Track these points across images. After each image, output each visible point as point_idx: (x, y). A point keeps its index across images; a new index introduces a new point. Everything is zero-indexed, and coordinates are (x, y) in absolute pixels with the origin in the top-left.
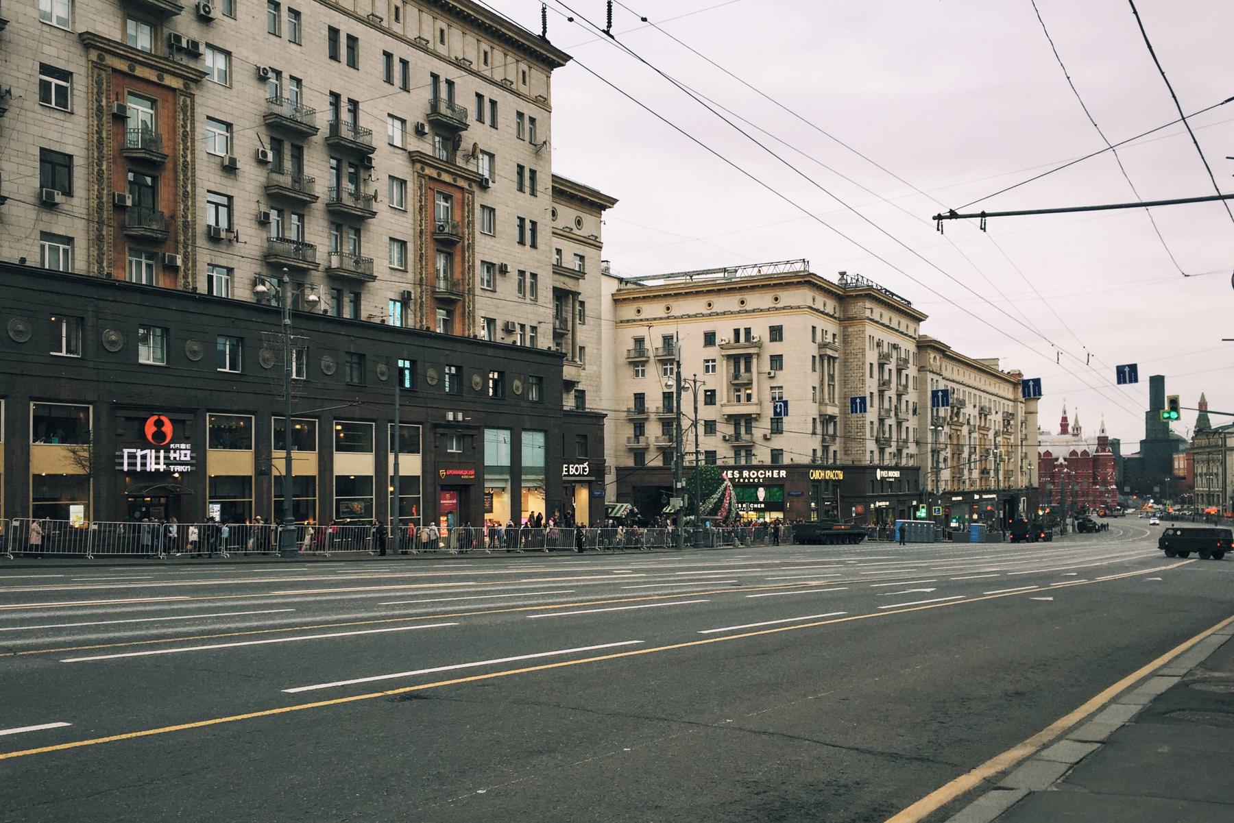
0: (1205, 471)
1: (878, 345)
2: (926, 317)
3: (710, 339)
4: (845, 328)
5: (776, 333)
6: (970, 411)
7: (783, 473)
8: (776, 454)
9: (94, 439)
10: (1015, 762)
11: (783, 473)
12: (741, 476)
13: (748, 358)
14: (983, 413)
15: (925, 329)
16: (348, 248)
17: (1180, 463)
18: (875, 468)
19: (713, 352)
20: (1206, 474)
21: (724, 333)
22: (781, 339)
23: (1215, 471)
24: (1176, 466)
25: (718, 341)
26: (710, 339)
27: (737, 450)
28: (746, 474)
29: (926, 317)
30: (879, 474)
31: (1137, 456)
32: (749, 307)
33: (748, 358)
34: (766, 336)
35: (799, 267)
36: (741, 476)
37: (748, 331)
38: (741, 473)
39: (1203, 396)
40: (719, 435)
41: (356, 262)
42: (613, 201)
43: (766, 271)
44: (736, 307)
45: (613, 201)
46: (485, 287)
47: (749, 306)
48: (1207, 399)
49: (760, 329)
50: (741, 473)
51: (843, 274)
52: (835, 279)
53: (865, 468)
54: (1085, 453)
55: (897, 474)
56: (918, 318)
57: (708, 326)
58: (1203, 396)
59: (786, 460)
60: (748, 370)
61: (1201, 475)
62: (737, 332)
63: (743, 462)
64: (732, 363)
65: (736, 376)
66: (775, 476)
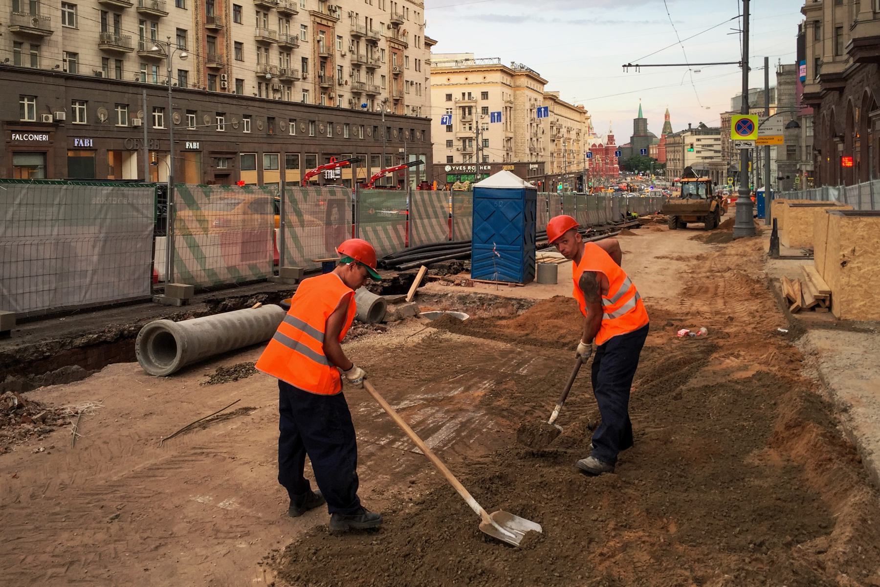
0: (672, 157)
1: (530, 100)
2: (547, 82)
3: (449, 97)
4: (515, 91)
5: (485, 95)
6: (563, 131)
7: (489, 167)
8: (485, 158)
9: (188, 120)
10: (599, 335)
11: (489, 167)
12: (467, 169)
13: (470, 108)
14: (569, 131)
15: (547, 89)
16: (263, 61)
17: (653, 151)
18: (529, 163)
19: (450, 104)
20: (673, 160)
21: (457, 95)
22: (487, 98)
23: (678, 157)
24: (651, 152)
25: (453, 98)
26: (449, 97)
27: (464, 155)
28: (469, 168)
29: (547, 82)
30: (531, 166)
31: (627, 146)
32: (470, 81)
33: (470, 108)
34: (479, 96)
35: (496, 62)
36: (467, 169)
37: (470, 94)
38: (467, 168)
39: (667, 111)
40: (455, 148)
41: (35, 20)
42: (436, 42)
43: (487, 62)
44: (463, 81)
45: (436, 42)
46: (67, 25)
47: (452, 82)
48: (670, 112)
49: (476, 94)
50: (467, 168)
51: (513, 63)
52: (509, 66)
53: (525, 163)
54: (601, 145)
55: (536, 166)
56: (543, 83)
57: (449, 91)
58: (667, 111)
59: (490, 161)
60: (470, 113)
61: (670, 160)
62: (464, 94)
63: (468, 162)
64: (461, 111)
65: (464, 118)
66: (485, 168)
